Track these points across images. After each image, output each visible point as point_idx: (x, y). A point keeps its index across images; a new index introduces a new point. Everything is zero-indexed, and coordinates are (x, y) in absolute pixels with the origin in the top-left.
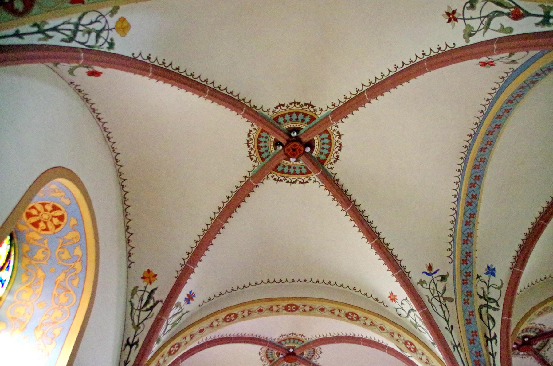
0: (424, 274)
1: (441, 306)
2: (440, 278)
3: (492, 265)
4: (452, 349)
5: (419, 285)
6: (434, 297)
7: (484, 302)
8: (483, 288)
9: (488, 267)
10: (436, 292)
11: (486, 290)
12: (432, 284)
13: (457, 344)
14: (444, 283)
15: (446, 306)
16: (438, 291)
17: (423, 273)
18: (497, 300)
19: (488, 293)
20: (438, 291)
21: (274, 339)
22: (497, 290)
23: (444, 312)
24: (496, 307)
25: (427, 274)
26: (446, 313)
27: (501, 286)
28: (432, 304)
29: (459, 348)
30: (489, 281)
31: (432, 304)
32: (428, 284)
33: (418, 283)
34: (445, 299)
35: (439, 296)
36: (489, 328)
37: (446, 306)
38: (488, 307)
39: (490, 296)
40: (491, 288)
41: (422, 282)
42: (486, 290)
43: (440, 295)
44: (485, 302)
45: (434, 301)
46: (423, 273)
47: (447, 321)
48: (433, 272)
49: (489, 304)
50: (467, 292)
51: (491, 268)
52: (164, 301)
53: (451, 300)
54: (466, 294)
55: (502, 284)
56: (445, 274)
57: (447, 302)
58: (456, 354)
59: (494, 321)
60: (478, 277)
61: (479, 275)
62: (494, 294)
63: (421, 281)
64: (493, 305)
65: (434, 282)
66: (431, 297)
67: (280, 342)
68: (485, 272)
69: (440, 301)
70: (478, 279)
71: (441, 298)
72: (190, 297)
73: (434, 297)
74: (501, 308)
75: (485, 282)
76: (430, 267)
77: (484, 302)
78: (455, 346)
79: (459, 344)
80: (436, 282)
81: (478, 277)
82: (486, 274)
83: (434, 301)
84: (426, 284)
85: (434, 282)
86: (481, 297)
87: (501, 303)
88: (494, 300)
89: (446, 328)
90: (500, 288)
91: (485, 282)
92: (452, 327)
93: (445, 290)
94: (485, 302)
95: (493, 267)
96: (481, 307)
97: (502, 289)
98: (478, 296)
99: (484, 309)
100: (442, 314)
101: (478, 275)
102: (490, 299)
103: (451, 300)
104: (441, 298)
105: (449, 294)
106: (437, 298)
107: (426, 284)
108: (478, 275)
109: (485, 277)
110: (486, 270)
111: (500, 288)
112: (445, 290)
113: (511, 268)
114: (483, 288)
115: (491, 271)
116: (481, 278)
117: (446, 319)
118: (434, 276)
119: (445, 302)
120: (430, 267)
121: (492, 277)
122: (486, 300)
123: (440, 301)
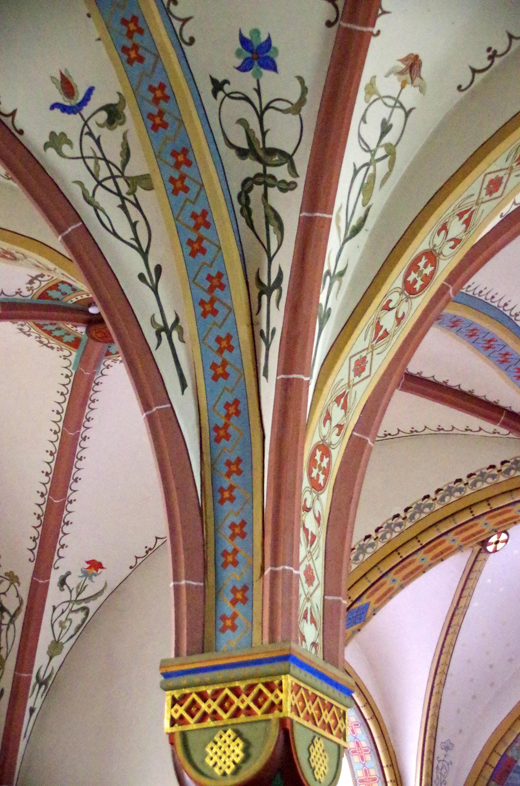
0: (57, 111)
1: (123, 207)
2: (103, 116)
3: (256, 32)
4: (151, 339)
5: (51, 151)
6: (100, 183)
7: (256, 168)
8: (242, 122)
9: (244, 41)
10: (102, 163)
11: (254, 124)
12: (87, 139)
13: (170, 321)
14: (120, 130)
15: (137, 205)
16: (108, 162)
17: (53, 107)
18: (290, 152)
19: (264, 134)
20: (108, 162)
21: (19, 293)
22: (290, 115)
23: (134, 226)
24: (289, 179)
25: (65, 109)
26: (141, 229)
27: (302, 101)
28: (96, 208)
29: (175, 335)
30: (258, 91)
31: (96, 208)
32: (76, 144)
33: (46, 146)
34: (134, 182)
35: (113, 177)
36: (268, 251)
37: (137, 205)
38: (265, 180)
39: (268, 145)
40: (269, 115)
41: (56, 141)
42: (254, 124)
43: (116, 172)
44: (259, 168)
45: (102, 197)
46: (53, 107)
47: (145, 255)
48: (81, 96)
49: (270, 170)
50: (174, 154)
51: (256, 44)
52: (53, 569)
53: (144, 181)
54: (171, 160)
55: (304, 90)
56: (115, 100)
57: (140, 193)
58: (163, 357)
59: (281, 228)
60: (218, 86)
61: (220, 79)
62: (283, 131)
63: (52, 134)
64: (281, 173)
65: (90, 134)
66: (90, 184)
67: (44, 295)
68: (239, 62)
69: (119, 194)
70: (221, 95)
71: (121, 182)
72: (32, 710)
73: (100, 183)
74: (301, 181)
75: (246, 99)
76: (67, 86)
77: (252, 167)
78: (165, 328)
79: (177, 320)
80: (96, 131)
81: (218, 86)
82: (243, 68)
83: (102, 197)
84: (70, 143)
85: (90, 134)
86: (242, 153)
87: (302, 161)
88: (282, 153)
89: (141, 277)
90: (296, 109)
91: (246, 99)
92: (159, 269)
93: (126, 154)
94: (259, 168)
95: (263, 38)
96: (247, 184)
97: (304, 111)
98: (233, 152)
99: (257, 190)
100: (127, 234)
101: (214, 81)
102: (272, 152)
103: (144, 181)
104: (121, 182)
105: (137, 167)
106: (109, 183)
107: (70, 143)
108: (214, 81)
109: (243, 83)
110: (238, 54)
111: (296, 109)
112: (126, 154)
113: (329, 24)
114: (242, 122)
115: (258, 55)
116: (227, 88)
117: (139, 249)
118: (87, 111)
119: (133, 192)
120: (67, 86)
121: (267, 74)
122: (259, 159)
123: (119, 194)
